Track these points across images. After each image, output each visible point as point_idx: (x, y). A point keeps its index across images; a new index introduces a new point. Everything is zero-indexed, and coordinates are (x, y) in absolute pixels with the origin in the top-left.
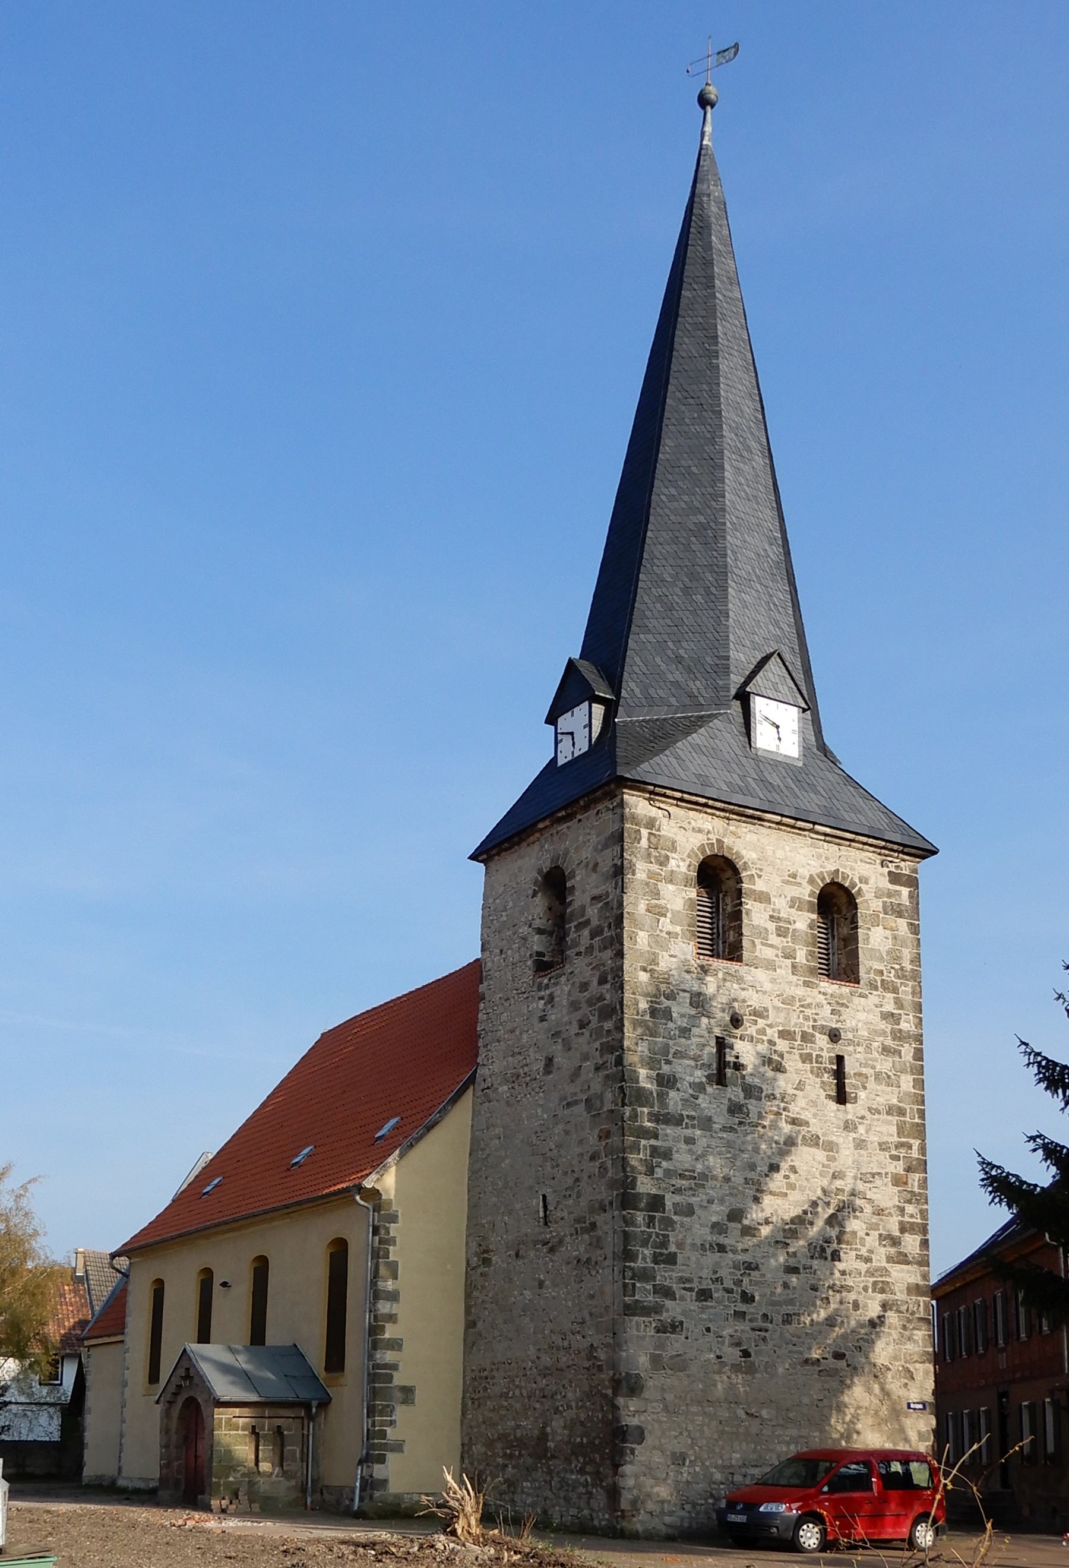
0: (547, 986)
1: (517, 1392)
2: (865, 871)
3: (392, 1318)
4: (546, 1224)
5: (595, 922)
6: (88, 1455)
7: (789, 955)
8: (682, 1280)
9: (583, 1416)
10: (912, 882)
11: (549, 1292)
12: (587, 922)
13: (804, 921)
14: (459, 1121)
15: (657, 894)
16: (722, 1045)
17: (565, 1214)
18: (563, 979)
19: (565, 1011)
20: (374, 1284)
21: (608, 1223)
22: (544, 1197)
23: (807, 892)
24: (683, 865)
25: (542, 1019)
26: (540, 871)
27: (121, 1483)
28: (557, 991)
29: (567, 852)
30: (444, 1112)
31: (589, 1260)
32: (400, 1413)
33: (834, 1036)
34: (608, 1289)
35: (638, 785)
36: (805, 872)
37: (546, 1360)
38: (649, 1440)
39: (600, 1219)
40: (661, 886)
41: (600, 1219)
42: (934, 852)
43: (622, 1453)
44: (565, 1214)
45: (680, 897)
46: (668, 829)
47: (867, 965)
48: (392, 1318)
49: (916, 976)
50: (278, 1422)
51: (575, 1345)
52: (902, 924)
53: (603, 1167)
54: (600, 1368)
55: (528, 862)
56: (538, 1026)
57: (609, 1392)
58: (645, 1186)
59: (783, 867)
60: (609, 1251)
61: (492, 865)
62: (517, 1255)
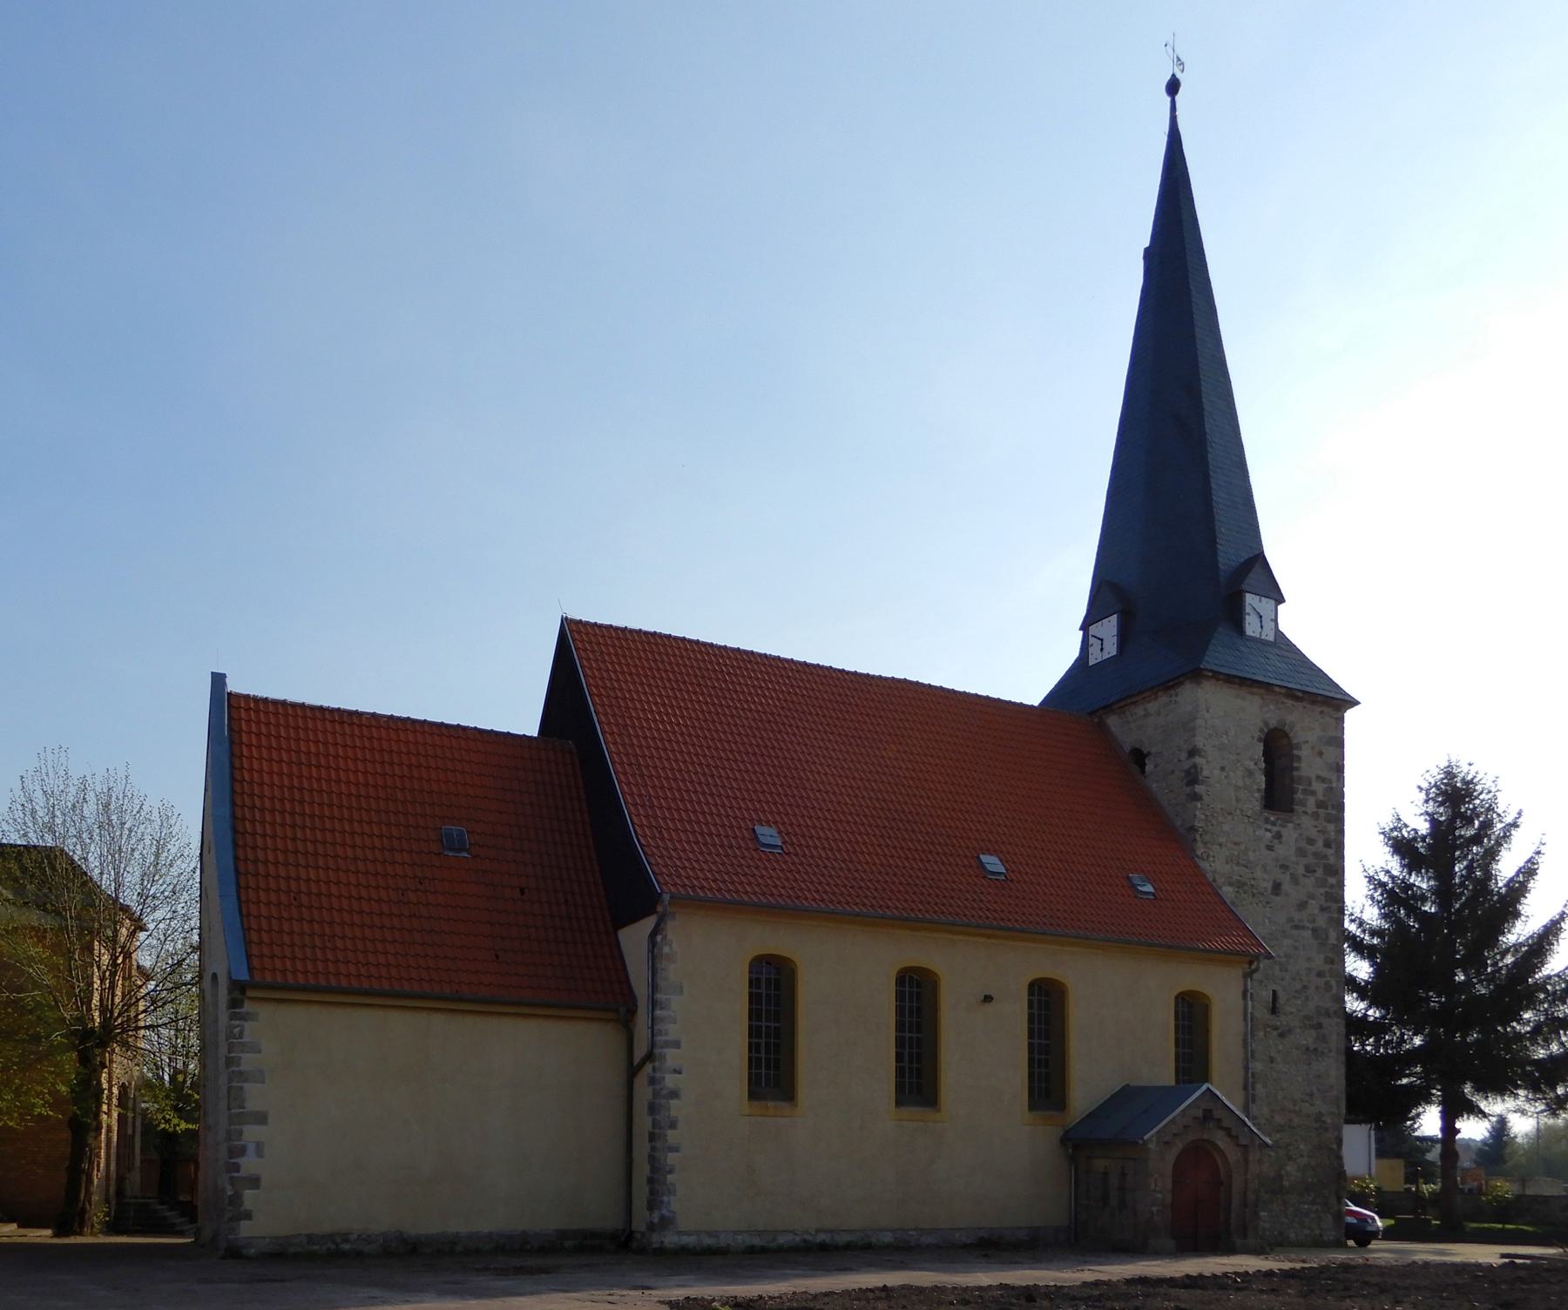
0: (1274, 824)
18: (1290, 825)
28: (1285, 832)
37: (1279, 1119)
39: (1325, 1021)
41: (1325, 1021)
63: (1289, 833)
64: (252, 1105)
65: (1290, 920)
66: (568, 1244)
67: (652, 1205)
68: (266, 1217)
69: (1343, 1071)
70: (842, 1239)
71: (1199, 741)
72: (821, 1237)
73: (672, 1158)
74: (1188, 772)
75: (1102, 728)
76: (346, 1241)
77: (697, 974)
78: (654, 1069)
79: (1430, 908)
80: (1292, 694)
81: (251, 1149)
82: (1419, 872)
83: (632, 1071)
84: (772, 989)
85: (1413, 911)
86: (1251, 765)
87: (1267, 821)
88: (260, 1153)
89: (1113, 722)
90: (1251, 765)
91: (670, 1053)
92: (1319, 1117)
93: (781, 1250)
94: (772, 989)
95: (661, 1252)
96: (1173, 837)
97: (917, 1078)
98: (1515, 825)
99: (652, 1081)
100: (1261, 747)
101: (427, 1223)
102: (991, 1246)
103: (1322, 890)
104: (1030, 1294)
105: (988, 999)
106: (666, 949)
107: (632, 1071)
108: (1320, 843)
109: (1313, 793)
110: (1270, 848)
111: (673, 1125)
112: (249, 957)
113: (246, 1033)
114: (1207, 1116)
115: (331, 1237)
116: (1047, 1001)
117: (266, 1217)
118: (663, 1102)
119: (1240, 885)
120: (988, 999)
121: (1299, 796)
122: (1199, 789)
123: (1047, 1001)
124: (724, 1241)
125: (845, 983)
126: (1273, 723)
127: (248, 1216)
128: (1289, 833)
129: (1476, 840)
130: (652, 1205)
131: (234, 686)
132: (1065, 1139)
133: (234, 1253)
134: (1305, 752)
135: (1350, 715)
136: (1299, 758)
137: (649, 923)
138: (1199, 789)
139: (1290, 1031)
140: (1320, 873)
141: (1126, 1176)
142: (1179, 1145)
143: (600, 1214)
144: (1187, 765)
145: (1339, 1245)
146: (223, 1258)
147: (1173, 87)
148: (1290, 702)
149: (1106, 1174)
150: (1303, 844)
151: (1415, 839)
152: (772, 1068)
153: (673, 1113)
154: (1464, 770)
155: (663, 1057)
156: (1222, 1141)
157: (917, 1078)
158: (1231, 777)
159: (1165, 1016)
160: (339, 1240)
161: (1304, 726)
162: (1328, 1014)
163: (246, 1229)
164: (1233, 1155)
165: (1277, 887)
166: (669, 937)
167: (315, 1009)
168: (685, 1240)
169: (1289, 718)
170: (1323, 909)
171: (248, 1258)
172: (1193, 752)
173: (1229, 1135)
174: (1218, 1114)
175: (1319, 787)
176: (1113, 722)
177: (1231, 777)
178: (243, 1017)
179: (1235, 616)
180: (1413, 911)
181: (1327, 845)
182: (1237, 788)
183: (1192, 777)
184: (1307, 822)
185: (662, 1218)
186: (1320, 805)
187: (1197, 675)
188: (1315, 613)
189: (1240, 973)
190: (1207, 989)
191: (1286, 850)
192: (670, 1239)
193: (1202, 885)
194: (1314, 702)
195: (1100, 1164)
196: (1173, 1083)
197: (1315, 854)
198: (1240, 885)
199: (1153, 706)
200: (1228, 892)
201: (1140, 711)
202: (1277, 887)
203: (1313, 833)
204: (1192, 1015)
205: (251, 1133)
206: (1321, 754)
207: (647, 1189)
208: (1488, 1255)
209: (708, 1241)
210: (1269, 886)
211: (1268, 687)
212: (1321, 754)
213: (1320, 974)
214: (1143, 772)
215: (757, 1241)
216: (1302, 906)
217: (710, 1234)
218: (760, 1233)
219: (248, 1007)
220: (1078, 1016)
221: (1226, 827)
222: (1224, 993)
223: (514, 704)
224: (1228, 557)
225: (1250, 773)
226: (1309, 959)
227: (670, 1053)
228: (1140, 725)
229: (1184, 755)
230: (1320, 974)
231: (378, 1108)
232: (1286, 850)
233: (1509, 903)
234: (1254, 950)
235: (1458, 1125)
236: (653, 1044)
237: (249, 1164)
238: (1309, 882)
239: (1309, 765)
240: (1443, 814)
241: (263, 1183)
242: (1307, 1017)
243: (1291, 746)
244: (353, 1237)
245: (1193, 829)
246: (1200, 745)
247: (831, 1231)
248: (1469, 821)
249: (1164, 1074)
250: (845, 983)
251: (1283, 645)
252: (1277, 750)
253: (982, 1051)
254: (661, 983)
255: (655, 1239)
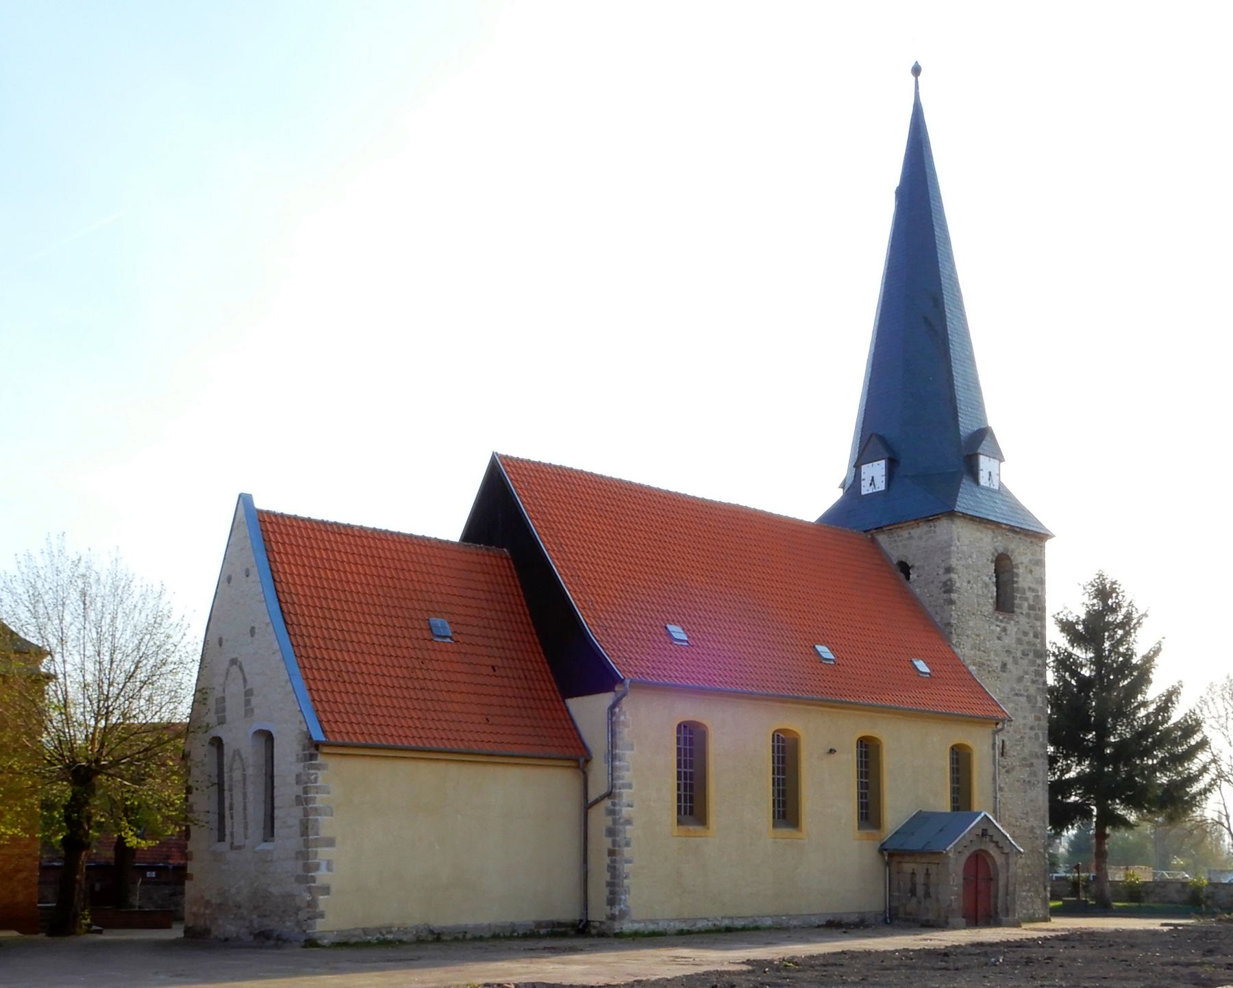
28: (1009, 627)
63: (1012, 628)
64: (324, 833)
65: (1013, 689)
66: (542, 931)
67: (612, 902)
68: (333, 919)
69: (1047, 796)
70: (739, 923)
71: (954, 562)
72: (726, 922)
73: (627, 867)
74: (945, 584)
75: (873, 540)
76: (390, 932)
77: (637, 735)
78: (614, 804)
79: (1086, 672)
80: (1012, 529)
81: (323, 866)
82: (1079, 646)
83: (587, 806)
84: (691, 743)
85: (1075, 674)
86: (987, 579)
87: (997, 619)
88: (329, 869)
89: (882, 539)
90: (987, 579)
91: (625, 791)
92: (1032, 829)
93: (700, 932)
94: (691, 743)
95: (620, 935)
96: (936, 631)
97: (786, 810)
98: (1145, 615)
99: (612, 812)
100: (993, 567)
101: (447, 918)
102: (835, 926)
104: (781, 967)
105: (832, 751)
106: (622, 718)
107: (587, 806)
108: (1031, 635)
109: (1026, 599)
110: (999, 638)
111: (628, 844)
112: (320, 722)
113: (320, 779)
114: (984, 833)
115: (379, 930)
116: (868, 751)
117: (333, 919)
118: (621, 828)
119: (981, 665)
120: (832, 751)
121: (1017, 601)
122: (954, 596)
123: (868, 751)
124: (662, 926)
125: (740, 742)
126: (1001, 550)
127: (322, 915)
128: (1012, 628)
129: (1122, 625)
130: (612, 902)
131: (261, 504)
132: (882, 850)
133: (311, 943)
134: (1021, 571)
135: (1049, 544)
136: (1017, 575)
137: (606, 699)
138: (954, 596)
139: (1013, 769)
140: (1031, 655)
141: (925, 872)
142: (967, 854)
143: (568, 912)
144: (944, 578)
145: (1046, 920)
146: (304, 947)
147: (916, 71)
148: (1011, 535)
149: (913, 873)
150: (1020, 636)
151: (1077, 623)
152: (692, 803)
153: (628, 836)
154: (1110, 577)
155: (620, 795)
156: (992, 850)
157: (786, 810)
158: (974, 586)
159: (946, 763)
160: (384, 932)
161: (1021, 554)
162: (1037, 757)
163: (320, 926)
164: (999, 859)
165: (1004, 665)
166: (624, 708)
167: (422, 764)
168: (636, 926)
169: (1012, 546)
170: (1033, 682)
171: (324, 947)
172: (949, 570)
173: (998, 846)
174: (990, 832)
175: (1030, 595)
176: (882, 539)
177: (974, 586)
178: (317, 767)
179: (973, 471)
180: (1075, 674)
181: (1036, 636)
182: (978, 596)
183: (948, 588)
184: (1023, 620)
185: (621, 911)
186: (1031, 608)
187: (951, 514)
188: (1023, 469)
189: (990, 731)
190: (969, 743)
191: (1009, 641)
192: (627, 926)
193: (958, 666)
194: (1026, 535)
195: (908, 867)
196: (949, 810)
197: (1028, 643)
198: (981, 665)
199: (916, 532)
200: (972, 668)
201: (905, 534)
202: (1004, 665)
203: (1027, 628)
204: (960, 759)
205: (323, 853)
206: (1031, 571)
207: (606, 891)
208: (1154, 924)
209: (651, 927)
210: (998, 665)
211: (998, 524)
213: (1032, 728)
214: (908, 578)
215: (685, 927)
216: (1020, 679)
217: (652, 921)
218: (685, 920)
219: (321, 759)
220: (889, 761)
221: (971, 624)
222: (980, 743)
223: (444, 515)
224: (966, 426)
225: (986, 585)
226: (1025, 718)
227: (625, 791)
228: (903, 544)
229: (941, 571)
230: (1032, 728)
231: (404, 831)
232: (1009, 641)
233: (1142, 675)
234: (1000, 716)
235: (1108, 831)
236: (613, 786)
237: (322, 876)
238: (1025, 662)
239: (1024, 580)
240: (1097, 604)
241: (333, 889)
242: (1024, 759)
243: (1013, 567)
244: (395, 929)
245: (949, 624)
246: (954, 565)
247: (731, 918)
248: (1113, 610)
249: (943, 803)
250: (740, 742)
251: (1002, 493)
252: (1003, 567)
253: (828, 788)
254: (619, 742)
255: (617, 926)
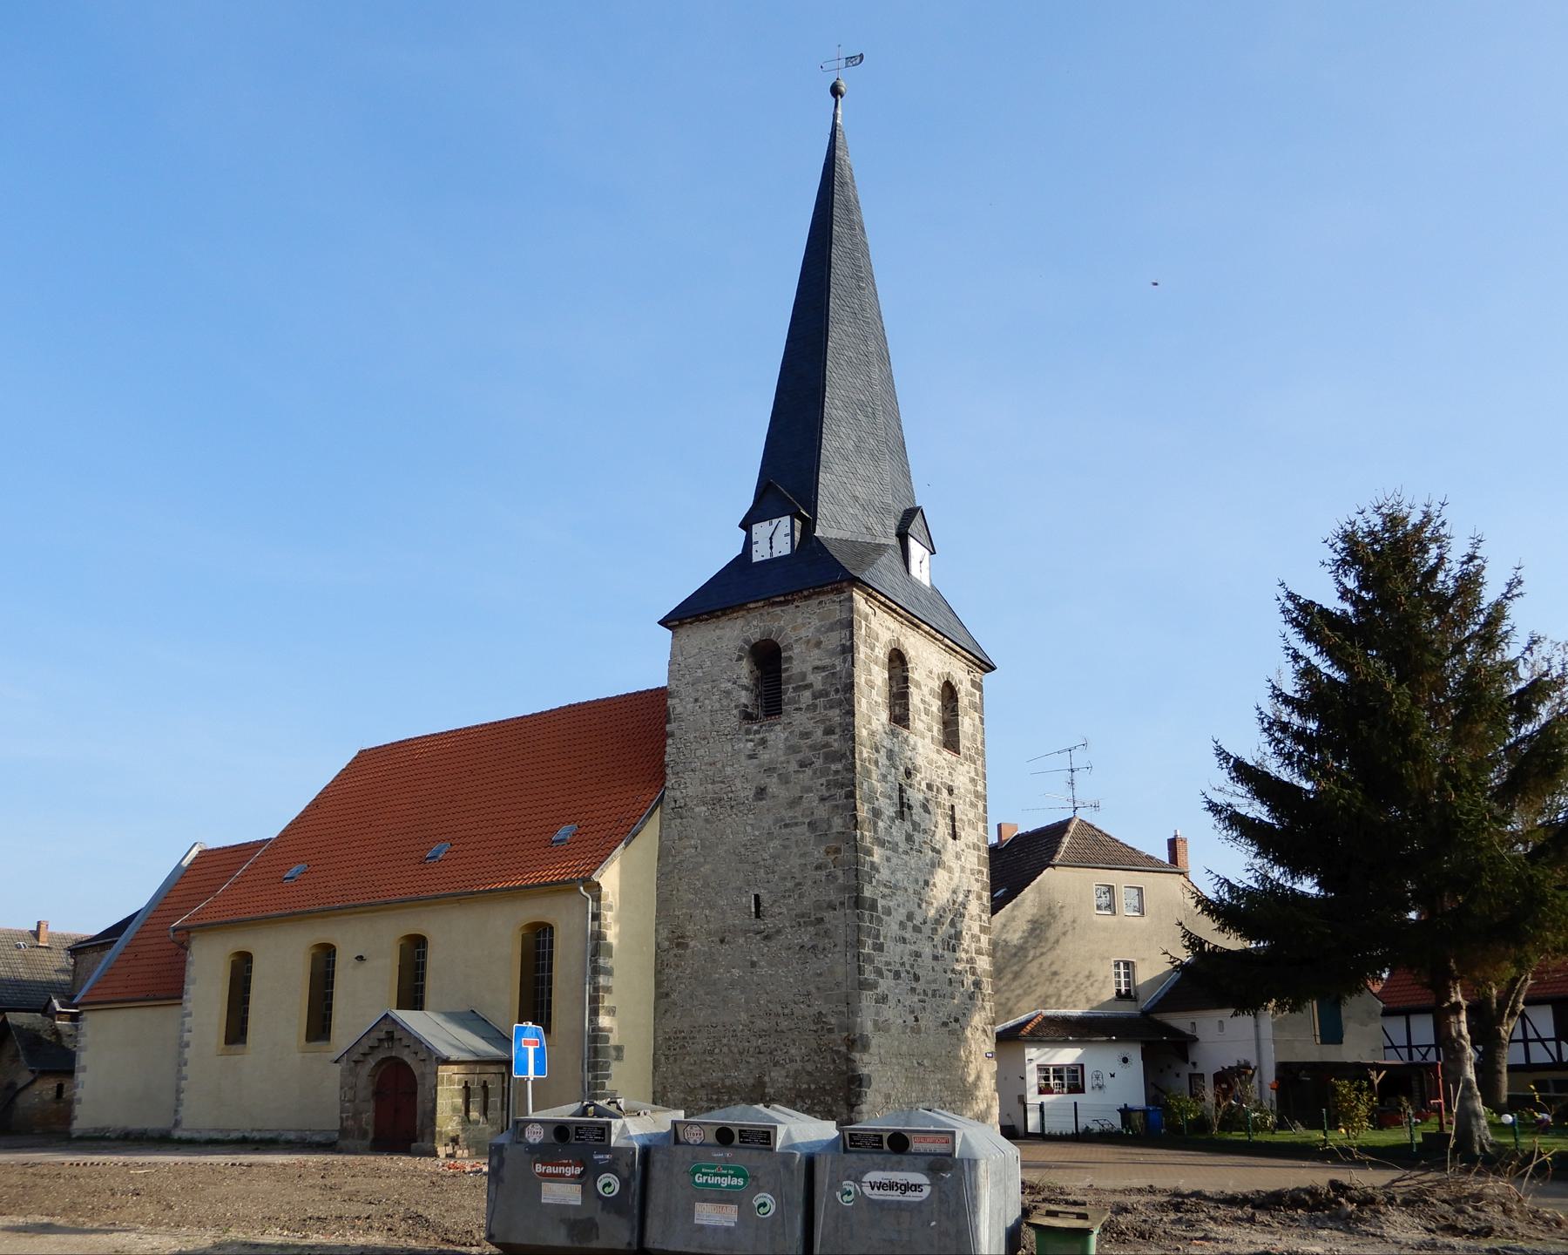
0: (757, 732)
1: (725, 1049)
2: (962, 676)
3: (608, 990)
4: (758, 916)
5: (818, 686)
6: (78, 1110)
7: (930, 730)
8: (888, 964)
9: (810, 1067)
10: (980, 688)
11: (764, 970)
12: (809, 686)
13: (936, 705)
14: (651, 832)
15: (869, 672)
16: (901, 790)
17: (784, 910)
18: (778, 728)
19: (780, 753)
20: (594, 961)
21: (837, 921)
22: (757, 897)
23: (936, 685)
24: (881, 653)
25: (751, 757)
26: (746, 641)
27: (177, 1134)
28: (771, 737)
29: (781, 630)
30: (644, 823)
31: (814, 947)
32: (614, 1068)
33: (951, 791)
34: (840, 970)
35: (864, 586)
36: (936, 671)
37: (761, 1024)
38: (874, 1086)
39: (828, 915)
40: (872, 666)
41: (828, 915)
42: (993, 668)
43: (859, 1096)
44: (784, 910)
45: (880, 675)
46: (874, 624)
47: (964, 743)
48: (608, 990)
49: (983, 755)
50: (485, 1077)
51: (797, 1012)
52: (976, 715)
53: (831, 878)
54: (830, 1031)
55: (731, 636)
56: (745, 762)
57: (843, 1049)
58: (867, 892)
59: (930, 663)
60: (841, 941)
61: (682, 632)
62: (722, 941)
93: (288, 1142)
103: (823, 780)
114: (390, 1036)
120: (360, 958)
142: (372, 1062)
150: (795, 740)
156: (408, 1058)
159: (511, 952)
165: (761, 792)
212: (818, 644)
